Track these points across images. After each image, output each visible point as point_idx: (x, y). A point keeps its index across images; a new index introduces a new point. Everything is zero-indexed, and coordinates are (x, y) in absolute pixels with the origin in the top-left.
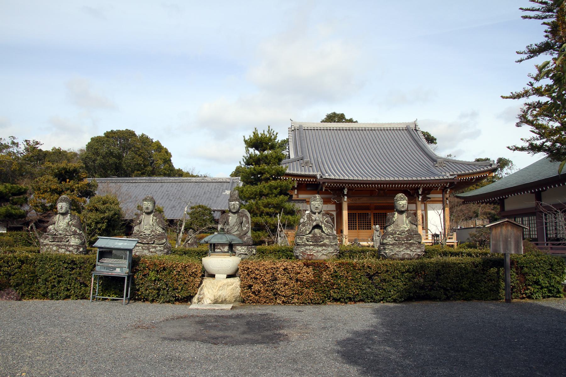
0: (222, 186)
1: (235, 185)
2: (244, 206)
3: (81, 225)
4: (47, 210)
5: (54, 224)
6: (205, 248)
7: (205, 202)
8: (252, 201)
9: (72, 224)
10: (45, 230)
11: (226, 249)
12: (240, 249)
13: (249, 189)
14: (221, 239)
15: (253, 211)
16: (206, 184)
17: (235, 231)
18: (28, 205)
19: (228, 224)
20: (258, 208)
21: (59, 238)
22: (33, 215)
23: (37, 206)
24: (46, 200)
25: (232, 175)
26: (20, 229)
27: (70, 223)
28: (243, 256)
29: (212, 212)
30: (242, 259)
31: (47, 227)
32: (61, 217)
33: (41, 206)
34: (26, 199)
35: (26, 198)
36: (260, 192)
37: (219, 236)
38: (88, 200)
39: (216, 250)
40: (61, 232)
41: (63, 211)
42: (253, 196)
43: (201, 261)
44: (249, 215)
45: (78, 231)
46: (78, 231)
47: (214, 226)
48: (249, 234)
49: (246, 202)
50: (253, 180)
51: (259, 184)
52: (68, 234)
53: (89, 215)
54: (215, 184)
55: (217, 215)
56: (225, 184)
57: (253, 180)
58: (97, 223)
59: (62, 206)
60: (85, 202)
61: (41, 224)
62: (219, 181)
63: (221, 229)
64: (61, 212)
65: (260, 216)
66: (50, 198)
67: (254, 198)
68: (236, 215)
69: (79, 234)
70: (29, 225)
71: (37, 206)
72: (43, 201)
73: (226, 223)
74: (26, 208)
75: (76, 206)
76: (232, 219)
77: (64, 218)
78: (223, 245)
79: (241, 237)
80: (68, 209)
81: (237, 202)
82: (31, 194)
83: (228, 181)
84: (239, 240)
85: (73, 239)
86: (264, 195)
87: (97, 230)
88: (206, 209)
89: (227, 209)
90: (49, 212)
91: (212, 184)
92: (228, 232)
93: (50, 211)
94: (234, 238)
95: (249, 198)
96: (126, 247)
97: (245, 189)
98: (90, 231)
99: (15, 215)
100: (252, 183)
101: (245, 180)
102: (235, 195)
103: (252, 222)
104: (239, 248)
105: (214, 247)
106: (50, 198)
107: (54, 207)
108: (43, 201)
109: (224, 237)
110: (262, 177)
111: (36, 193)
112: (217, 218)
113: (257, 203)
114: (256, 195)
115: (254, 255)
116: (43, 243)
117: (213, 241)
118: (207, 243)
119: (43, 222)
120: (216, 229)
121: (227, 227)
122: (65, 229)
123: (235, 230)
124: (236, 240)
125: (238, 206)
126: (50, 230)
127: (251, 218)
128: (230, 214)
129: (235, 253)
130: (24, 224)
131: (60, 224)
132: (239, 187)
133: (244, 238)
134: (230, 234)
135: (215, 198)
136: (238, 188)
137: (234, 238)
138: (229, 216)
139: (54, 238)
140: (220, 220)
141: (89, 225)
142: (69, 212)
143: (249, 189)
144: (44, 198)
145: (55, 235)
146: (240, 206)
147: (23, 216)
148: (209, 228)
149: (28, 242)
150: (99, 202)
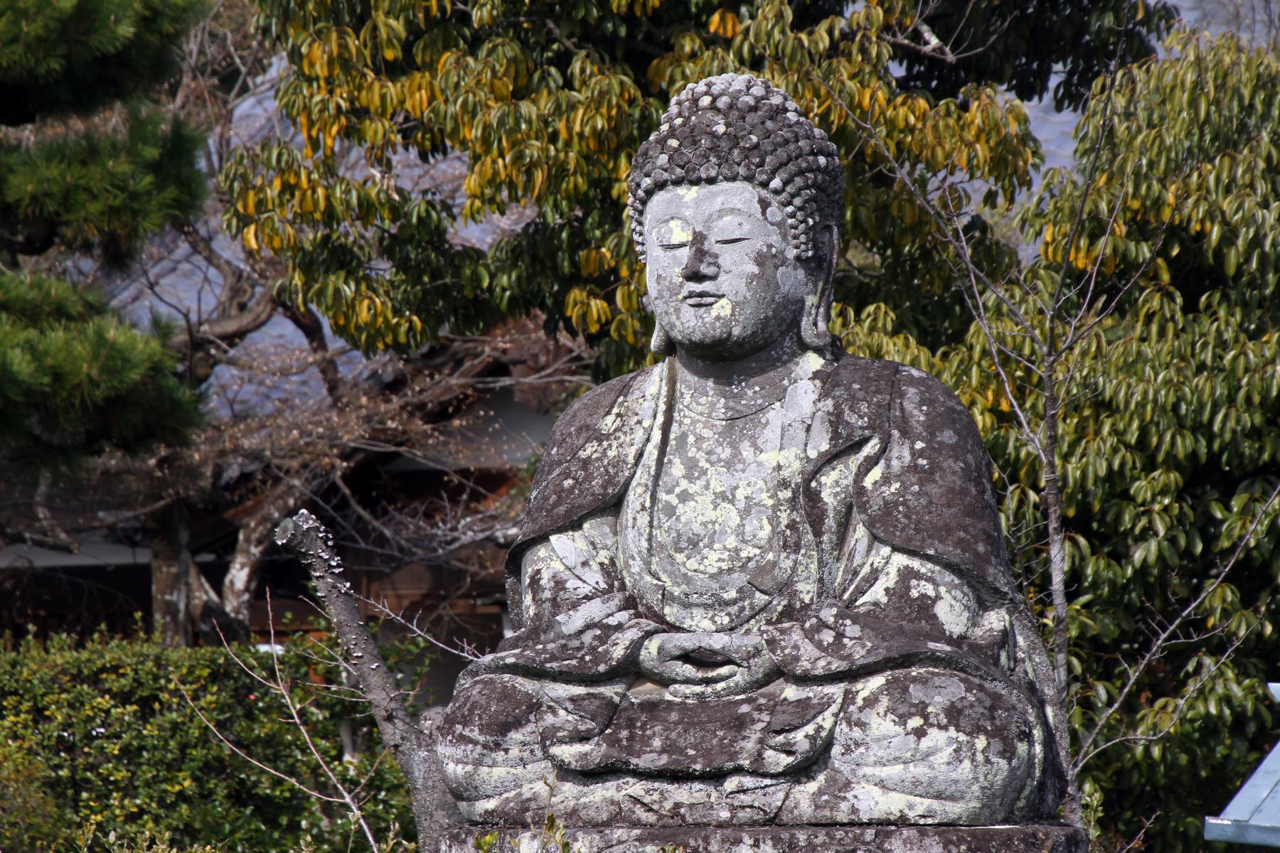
3: (986, 516)
4: (480, 312)
5: (612, 506)
9: (856, 499)
10: (471, 606)
18: (202, 246)
21: (693, 714)
22: (282, 391)
23: (341, 258)
24: (449, 167)
26: (112, 602)
27: (833, 485)
31: (516, 554)
32: (702, 402)
33: (391, 247)
34: (175, 158)
35: (180, 146)
38: (1056, 133)
40: (702, 629)
41: (727, 309)
45: (951, 613)
46: (951, 613)
52: (809, 657)
53: (1095, 354)
58: (1207, 479)
59: (705, 236)
60: (1009, 161)
61: (400, 527)
64: (689, 322)
66: (512, 129)
69: (972, 658)
70: (226, 548)
71: (341, 258)
72: (408, 173)
74: (178, 291)
75: (879, 229)
77: (740, 423)
80: (792, 279)
82: (229, 81)
85: (881, 724)
87: (1217, 594)
90: (500, 343)
93: (532, 315)
96: (51, 553)
98: (1114, 601)
99: (37, 401)
106: (512, 129)
107: (574, 255)
108: (408, 173)
111: (319, 56)
116: (461, 793)
119: (426, 488)
122: (759, 576)
126: (560, 601)
130: (158, 530)
131: (695, 514)
139: (610, 714)
141: (1097, 522)
142: (813, 327)
144: (431, 139)
145: (630, 670)
147: (150, 408)
149: (241, 795)
150: (1229, 141)
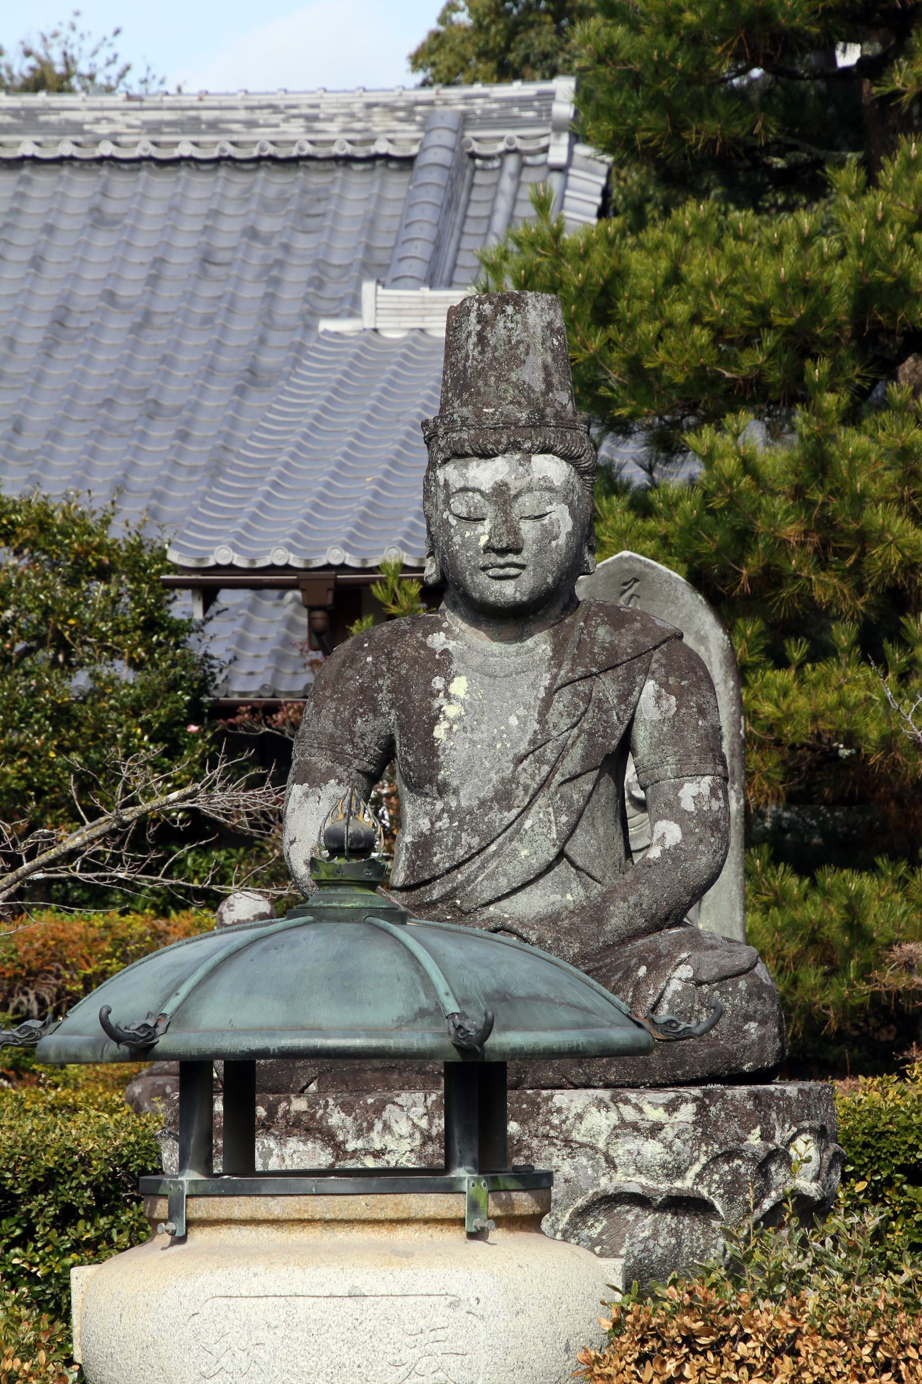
0: (306, 218)
1: (500, 213)
2: (642, 507)
6: (92, 1130)
7: (70, 449)
8: (751, 432)
11: (407, 1125)
12: (598, 1134)
13: (702, 265)
14: (345, 984)
15: (772, 577)
16: (81, 188)
17: (529, 873)
19: (426, 779)
20: (837, 542)
25: (440, 58)
28: (643, 1226)
29: (184, 606)
30: (640, 1279)
36: (865, 295)
37: (311, 944)
39: (275, 1153)
42: (773, 362)
43: (61, 1311)
44: (707, 636)
47: (222, 799)
48: (721, 913)
49: (666, 445)
50: (765, 128)
51: (847, 176)
54: (200, 189)
55: (252, 649)
56: (355, 192)
57: (765, 128)
62: (261, 140)
63: (336, 844)
65: (870, 649)
67: (776, 399)
68: (540, 644)
73: (398, 761)
76: (487, 701)
78: (360, 1072)
79: (606, 960)
81: (551, 469)
83: (398, 137)
84: (591, 995)
86: (431, 1014)
88: (92, 561)
89: (393, 549)
91: (161, 186)
92: (433, 897)
94: (519, 969)
95: (711, 398)
97: (644, 268)
100: (750, 176)
101: (650, 126)
102: (514, 356)
103: (762, 737)
104: (584, 1111)
105: (230, 1100)
109: (376, 958)
110: (902, 78)
112: (245, 681)
113: (818, 463)
114: (801, 344)
115: (811, 1210)
117: (230, 1021)
118: (140, 1047)
120: (251, 845)
121: (418, 818)
123: (531, 852)
124: (553, 1009)
125: (562, 519)
127: (742, 673)
128: (454, 635)
129: (538, 1182)
132: (552, 242)
133: (659, 964)
134: (457, 912)
135: (217, 397)
136: (542, 262)
137: (519, 969)
138: (442, 664)
140: (319, 722)
143: (702, 265)
146: (587, 537)
148: (155, 839)
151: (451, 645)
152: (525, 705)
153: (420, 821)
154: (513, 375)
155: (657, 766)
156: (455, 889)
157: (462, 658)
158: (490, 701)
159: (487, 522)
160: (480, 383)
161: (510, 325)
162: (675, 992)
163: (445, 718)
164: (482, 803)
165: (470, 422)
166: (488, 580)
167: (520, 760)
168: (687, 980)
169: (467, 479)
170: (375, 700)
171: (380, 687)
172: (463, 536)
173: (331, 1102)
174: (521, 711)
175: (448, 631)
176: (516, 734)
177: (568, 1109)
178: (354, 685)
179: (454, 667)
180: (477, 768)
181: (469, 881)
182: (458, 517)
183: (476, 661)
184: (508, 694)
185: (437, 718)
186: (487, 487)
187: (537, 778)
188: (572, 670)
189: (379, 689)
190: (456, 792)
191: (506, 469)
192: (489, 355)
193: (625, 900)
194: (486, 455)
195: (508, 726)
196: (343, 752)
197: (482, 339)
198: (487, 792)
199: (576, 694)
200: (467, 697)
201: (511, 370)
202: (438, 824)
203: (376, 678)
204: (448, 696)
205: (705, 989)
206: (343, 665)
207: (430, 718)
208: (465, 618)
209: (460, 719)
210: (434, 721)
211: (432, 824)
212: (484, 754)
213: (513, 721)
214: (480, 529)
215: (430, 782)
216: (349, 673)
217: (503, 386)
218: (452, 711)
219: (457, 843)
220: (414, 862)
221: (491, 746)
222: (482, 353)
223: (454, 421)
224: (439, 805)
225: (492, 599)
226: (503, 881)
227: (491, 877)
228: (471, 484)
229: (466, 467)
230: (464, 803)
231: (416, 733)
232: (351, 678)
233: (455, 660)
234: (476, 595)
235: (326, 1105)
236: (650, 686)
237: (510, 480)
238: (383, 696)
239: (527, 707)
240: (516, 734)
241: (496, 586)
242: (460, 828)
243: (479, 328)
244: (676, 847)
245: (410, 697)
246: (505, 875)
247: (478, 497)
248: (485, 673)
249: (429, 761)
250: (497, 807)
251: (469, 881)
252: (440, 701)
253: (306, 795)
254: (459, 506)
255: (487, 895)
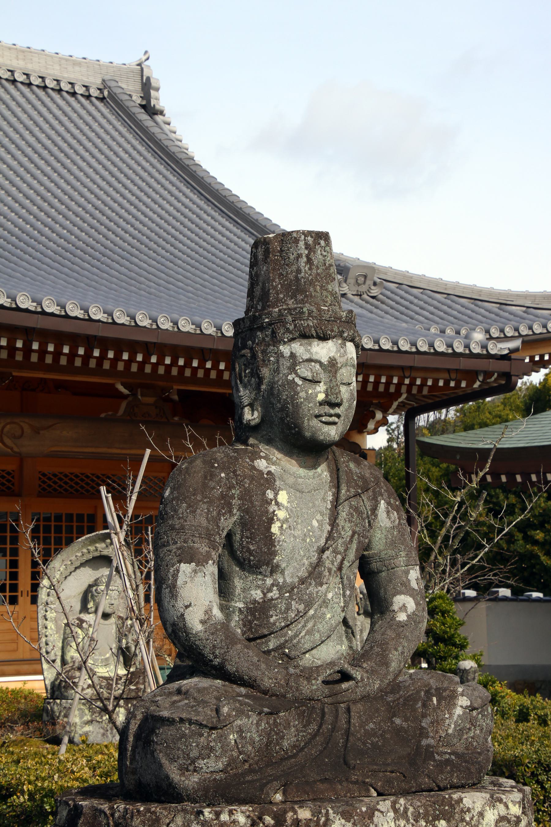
138: (269, 481)
151: (273, 468)
152: (321, 513)
153: (253, 592)
154: (329, 286)
155: (393, 558)
156: (286, 641)
157: (281, 478)
158: (301, 509)
159: (322, 384)
160: (312, 289)
161: (325, 254)
162: (459, 716)
163: (278, 519)
164: (302, 581)
165: (314, 314)
166: (320, 424)
167: (322, 550)
168: (467, 707)
169: (311, 353)
170: (230, 504)
171: (233, 494)
172: (307, 393)
173: (331, 811)
174: (319, 517)
175: (266, 458)
176: (318, 533)
177: (473, 808)
178: (218, 491)
179: (277, 483)
180: (296, 556)
181: (296, 636)
182: (304, 379)
183: (291, 480)
184: (311, 505)
185: (272, 519)
186: (325, 360)
187: (335, 564)
188: (348, 490)
189: (233, 497)
190: (283, 572)
191: (334, 349)
192: (314, 271)
193: (396, 650)
194: (324, 338)
195: (312, 527)
196: (214, 541)
197: (309, 261)
198: (303, 573)
199: (351, 507)
200: (289, 505)
201: (328, 283)
202: (270, 595)
203: (230, 488)
204: (277, 504)
205: (475, 713)
206: (206, 477)
207: (268, 519)
208: (280, 450)
209: (286, 520)
210: (271, 521)
211: (265, 594)
212: (300, 546)
213: (315, 523)
214: (318, 389)
215: (267, 564)
216: (212, 484)
217: (325, 293)
218: (281, 514)
219: (288, 608)
220: (250, 622)
221: (304, 540)
222: (310, 269)
223: (303, 313)
224: (269, 581)
225: (322, 438)
226: (317, 636)
227: (308, 633)
228: (315, 357)
229: (310, 345)
230: (289, 580)
231: (258, 529)
232: (214, 488)
233: (277, 479)
234: (308, 434)
235: (327, 813)
236: (383, 504)
237: (337, 356)
238: (235, 502)
239: (322, 514)
240: (318, 533)
241: (326, 428)
242: (290, 597)
243: (306, 252)
244: (414, 613)
245: (252, 503)
246: (318, 632)
247: (318, 366)
248: (296, 489)
249: (269, 549)
250: (314, 583)
251: (296, 636)
252: (272, 507)
253: (195, 571)
254: (304, 371)
255: (307, 646)
